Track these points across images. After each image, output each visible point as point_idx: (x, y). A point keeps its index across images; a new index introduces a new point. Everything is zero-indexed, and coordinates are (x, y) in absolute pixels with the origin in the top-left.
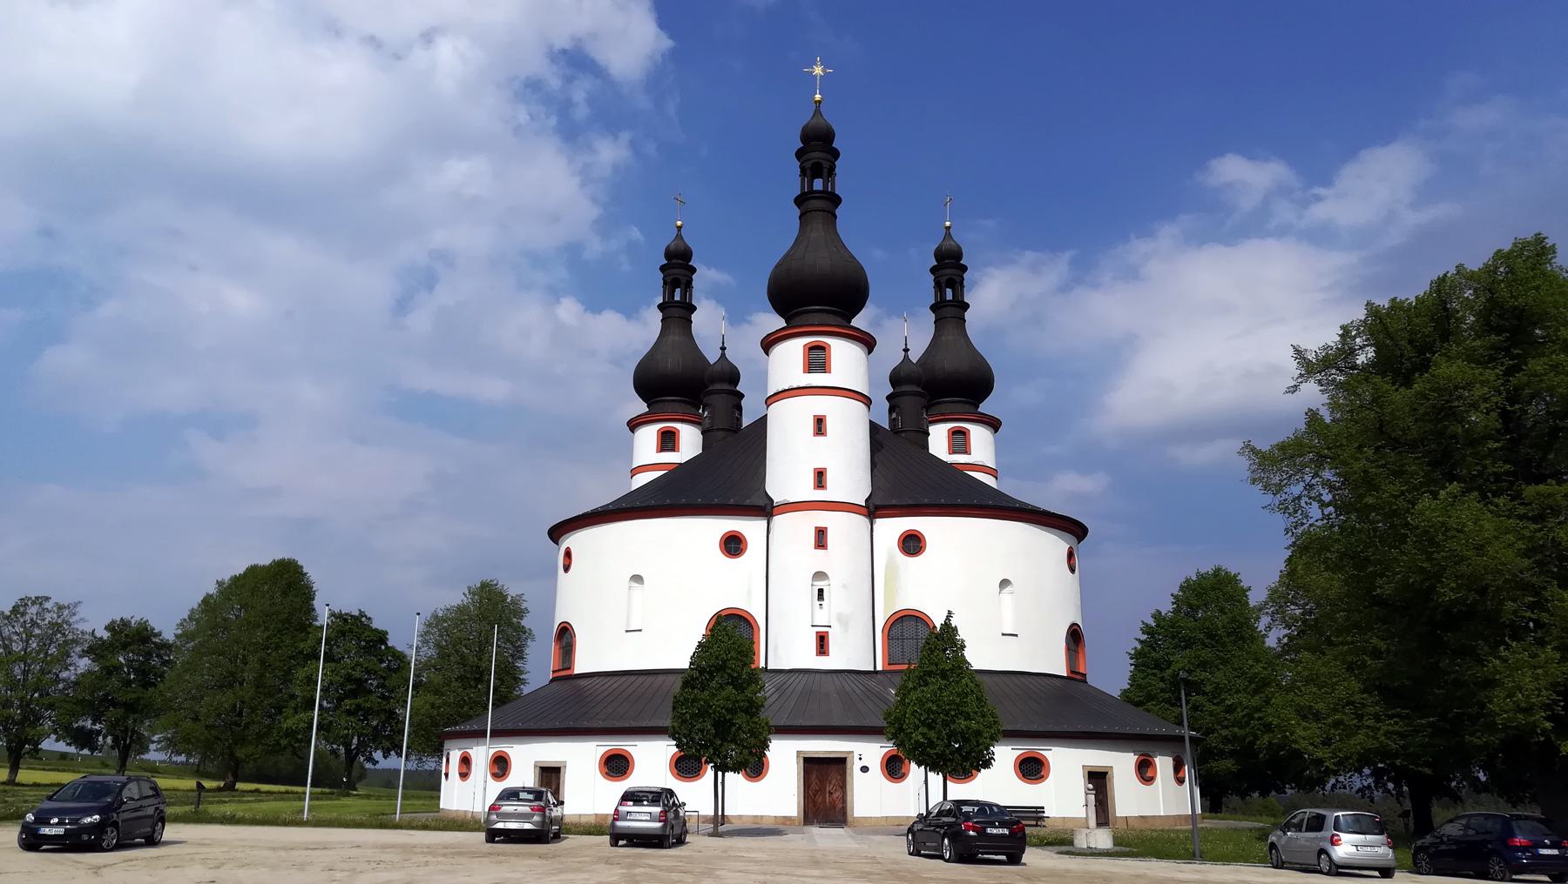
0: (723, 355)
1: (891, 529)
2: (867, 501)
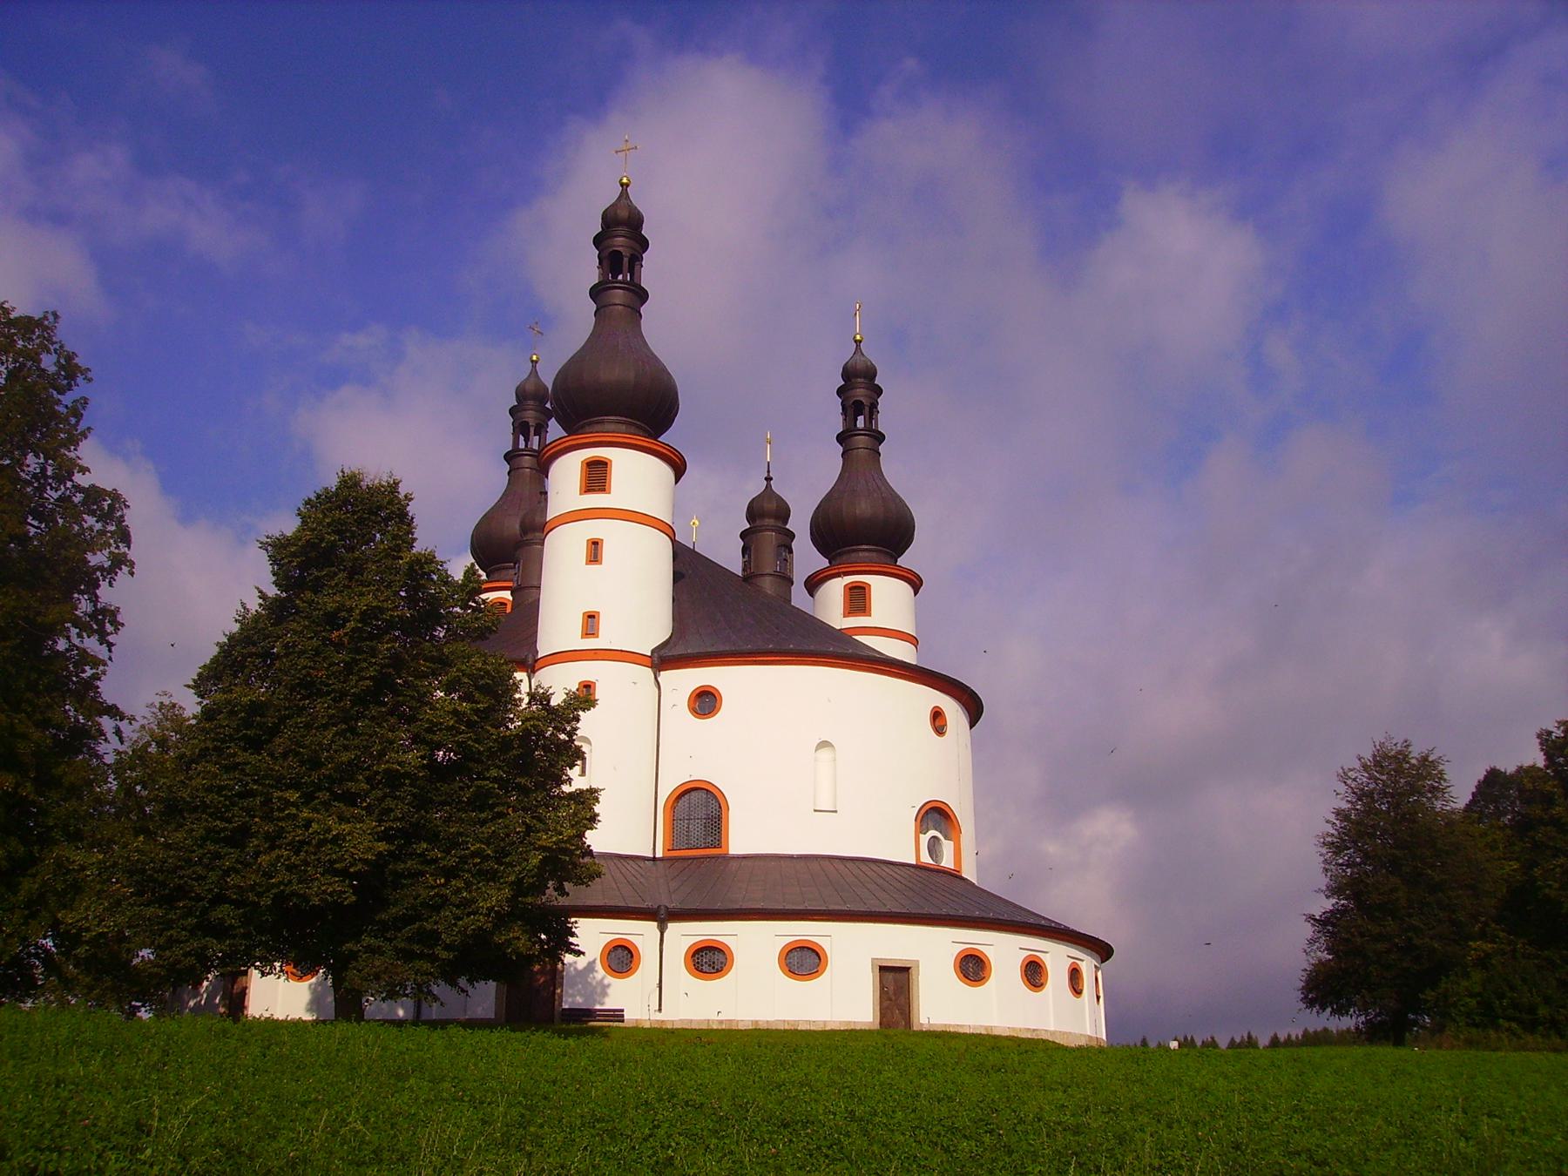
0: (768, 487)
2: (653, 651)
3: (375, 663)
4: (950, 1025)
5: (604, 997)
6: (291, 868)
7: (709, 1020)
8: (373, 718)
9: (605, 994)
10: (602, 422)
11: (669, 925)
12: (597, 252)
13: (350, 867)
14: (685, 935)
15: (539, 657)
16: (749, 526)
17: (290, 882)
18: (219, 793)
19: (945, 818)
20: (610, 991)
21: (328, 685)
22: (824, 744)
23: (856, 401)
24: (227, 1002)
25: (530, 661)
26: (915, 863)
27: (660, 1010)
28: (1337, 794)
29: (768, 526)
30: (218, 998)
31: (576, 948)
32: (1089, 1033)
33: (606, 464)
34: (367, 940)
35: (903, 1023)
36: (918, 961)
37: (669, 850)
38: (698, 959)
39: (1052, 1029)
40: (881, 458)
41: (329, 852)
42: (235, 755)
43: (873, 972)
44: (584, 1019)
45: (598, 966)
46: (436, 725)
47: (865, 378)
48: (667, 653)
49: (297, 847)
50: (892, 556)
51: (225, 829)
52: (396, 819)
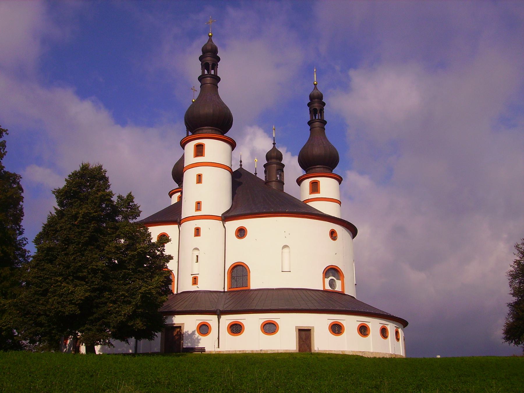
0: (274, 147)
1: (233, 225)
2: (222, 215)
3: (89, 232)
4: (332, 351)
5: (198, 343)
6: (58, 303)
7: (236, 351)
8: (89, 250)
9: (198, 342)
10: (202, 129)
11: (222, 316)
12: (201, 63)
13: (76, 302)
14: (227, 320)
15: (182, 219)
16: (267, 162)
17: (58, 307)
18: (38, 278)
19: (336, 271)
20: (200, 341)
21: (74, 240)
22: (285, 246)
23: (314, 108)
24: (74, 350)
25: (179, 221)
26: (322, 289)
27: (219, 347)
28: (514, 254)
29: (274, 162)
30: (72, 348)
31: (396, 326)
32: (391, 353)
33: (203, 145)
34: (87, 326)
35: (309, 350)
36: (314, 327)
37: (229, 288)
38: (232, 328)
39: (372, 351)
40: (325, 131)
41: (70, 297)
42: (43, 265)
43: (296, 331)
44: (190, 351)
45: (196, 333)
46: (109, 251)
47: (318, 99)
48: (228, 215)
49: (61, 296)
50: (329, 169)
51: (39, 291)
52: (96, 285)
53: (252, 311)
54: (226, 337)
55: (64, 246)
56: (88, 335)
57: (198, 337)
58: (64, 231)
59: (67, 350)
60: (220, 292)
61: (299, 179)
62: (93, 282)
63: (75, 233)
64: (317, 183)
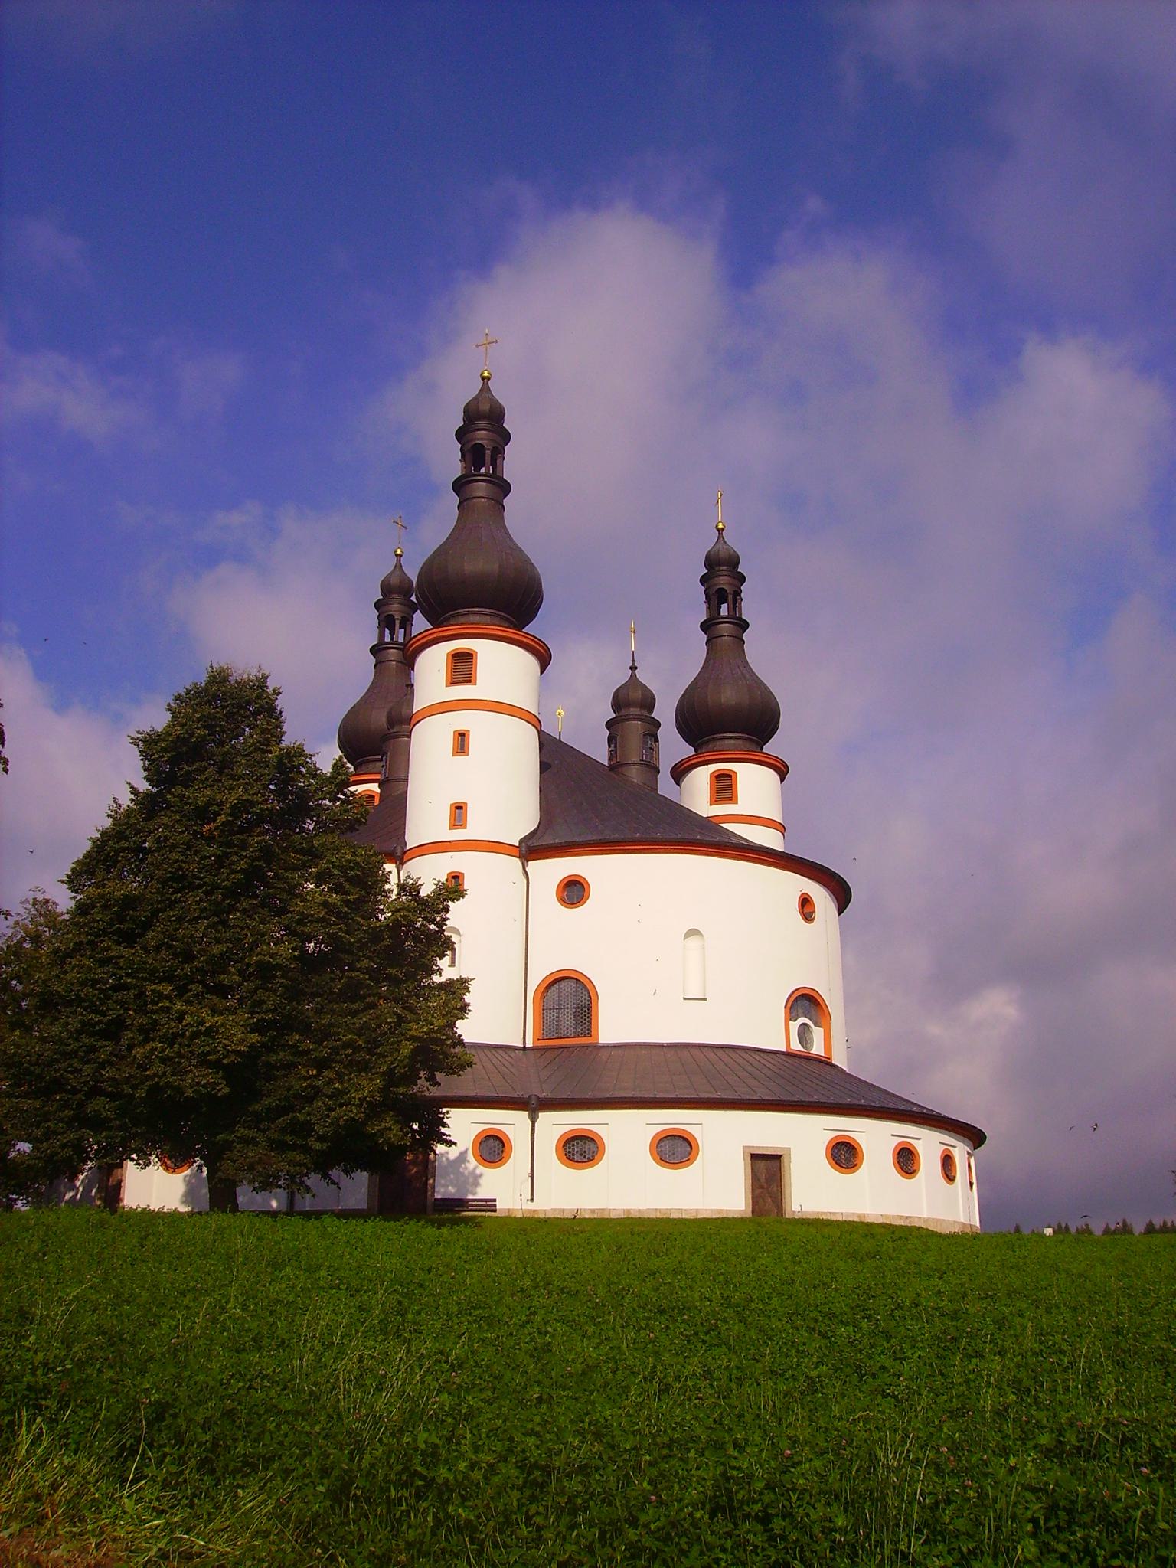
0: (633, 676)
1: (552, 871)
2: (521, 841)
4: (834, 1214)
9: (476, 1184)
14: (556, 1124)
15: (408, 848)
17: (164, 1074)
20: (481, 1181)
21: (200, 879)
22: (693, 933)
27: (532, 1199)
30: (94, 1191)
39: (925, 1216)
42: (108, 949)
43: (744, 1159)
45: (470, 1156)
49: (171, 1039)
51: (99, 1022)
52: (268, 1011)
53: (626, 1103)
54: (553, 1171)
55: (172, 893)
56: (247, 1157)
57: (475, 1168)
58: (171, 852)
59: (76, 1194)
60: (515, 1048)
61: (680, 767)
62: (262, 1002)
63: (202, 859)
64: (730, 776)
